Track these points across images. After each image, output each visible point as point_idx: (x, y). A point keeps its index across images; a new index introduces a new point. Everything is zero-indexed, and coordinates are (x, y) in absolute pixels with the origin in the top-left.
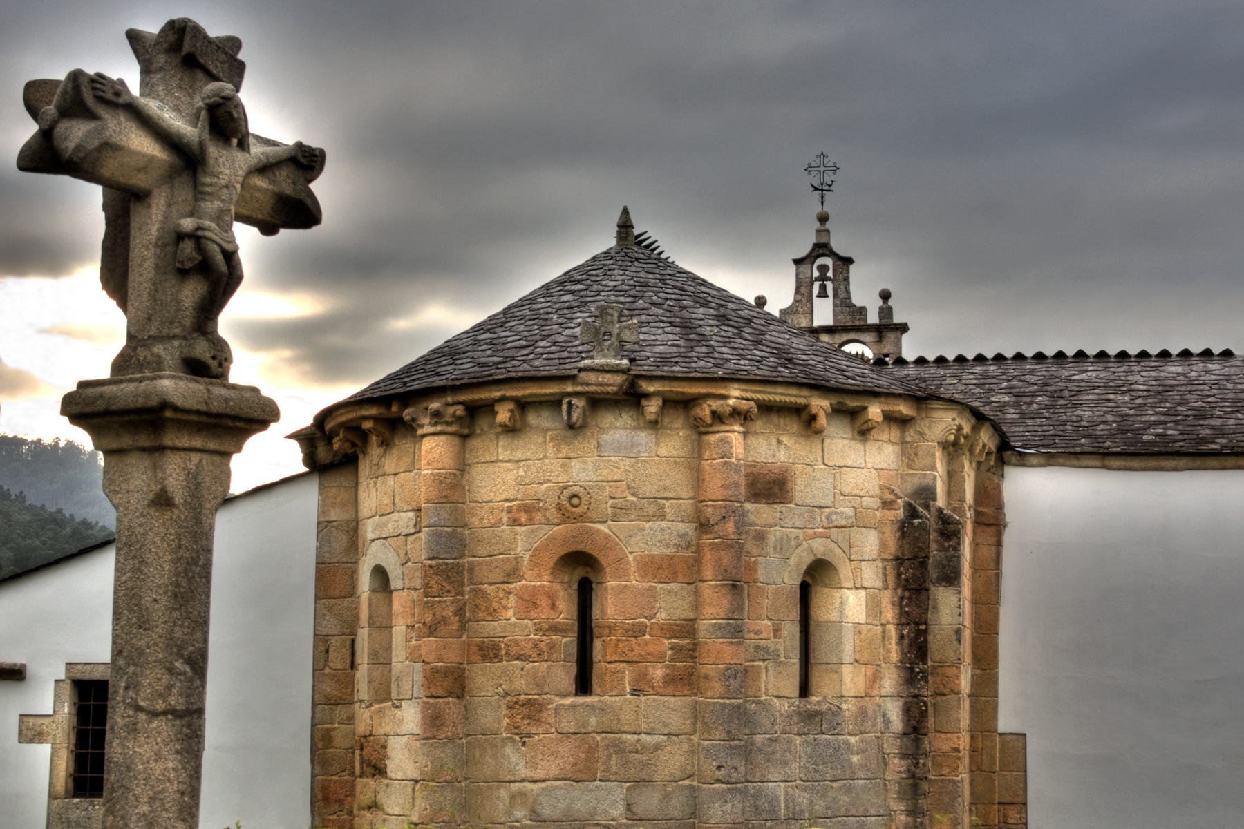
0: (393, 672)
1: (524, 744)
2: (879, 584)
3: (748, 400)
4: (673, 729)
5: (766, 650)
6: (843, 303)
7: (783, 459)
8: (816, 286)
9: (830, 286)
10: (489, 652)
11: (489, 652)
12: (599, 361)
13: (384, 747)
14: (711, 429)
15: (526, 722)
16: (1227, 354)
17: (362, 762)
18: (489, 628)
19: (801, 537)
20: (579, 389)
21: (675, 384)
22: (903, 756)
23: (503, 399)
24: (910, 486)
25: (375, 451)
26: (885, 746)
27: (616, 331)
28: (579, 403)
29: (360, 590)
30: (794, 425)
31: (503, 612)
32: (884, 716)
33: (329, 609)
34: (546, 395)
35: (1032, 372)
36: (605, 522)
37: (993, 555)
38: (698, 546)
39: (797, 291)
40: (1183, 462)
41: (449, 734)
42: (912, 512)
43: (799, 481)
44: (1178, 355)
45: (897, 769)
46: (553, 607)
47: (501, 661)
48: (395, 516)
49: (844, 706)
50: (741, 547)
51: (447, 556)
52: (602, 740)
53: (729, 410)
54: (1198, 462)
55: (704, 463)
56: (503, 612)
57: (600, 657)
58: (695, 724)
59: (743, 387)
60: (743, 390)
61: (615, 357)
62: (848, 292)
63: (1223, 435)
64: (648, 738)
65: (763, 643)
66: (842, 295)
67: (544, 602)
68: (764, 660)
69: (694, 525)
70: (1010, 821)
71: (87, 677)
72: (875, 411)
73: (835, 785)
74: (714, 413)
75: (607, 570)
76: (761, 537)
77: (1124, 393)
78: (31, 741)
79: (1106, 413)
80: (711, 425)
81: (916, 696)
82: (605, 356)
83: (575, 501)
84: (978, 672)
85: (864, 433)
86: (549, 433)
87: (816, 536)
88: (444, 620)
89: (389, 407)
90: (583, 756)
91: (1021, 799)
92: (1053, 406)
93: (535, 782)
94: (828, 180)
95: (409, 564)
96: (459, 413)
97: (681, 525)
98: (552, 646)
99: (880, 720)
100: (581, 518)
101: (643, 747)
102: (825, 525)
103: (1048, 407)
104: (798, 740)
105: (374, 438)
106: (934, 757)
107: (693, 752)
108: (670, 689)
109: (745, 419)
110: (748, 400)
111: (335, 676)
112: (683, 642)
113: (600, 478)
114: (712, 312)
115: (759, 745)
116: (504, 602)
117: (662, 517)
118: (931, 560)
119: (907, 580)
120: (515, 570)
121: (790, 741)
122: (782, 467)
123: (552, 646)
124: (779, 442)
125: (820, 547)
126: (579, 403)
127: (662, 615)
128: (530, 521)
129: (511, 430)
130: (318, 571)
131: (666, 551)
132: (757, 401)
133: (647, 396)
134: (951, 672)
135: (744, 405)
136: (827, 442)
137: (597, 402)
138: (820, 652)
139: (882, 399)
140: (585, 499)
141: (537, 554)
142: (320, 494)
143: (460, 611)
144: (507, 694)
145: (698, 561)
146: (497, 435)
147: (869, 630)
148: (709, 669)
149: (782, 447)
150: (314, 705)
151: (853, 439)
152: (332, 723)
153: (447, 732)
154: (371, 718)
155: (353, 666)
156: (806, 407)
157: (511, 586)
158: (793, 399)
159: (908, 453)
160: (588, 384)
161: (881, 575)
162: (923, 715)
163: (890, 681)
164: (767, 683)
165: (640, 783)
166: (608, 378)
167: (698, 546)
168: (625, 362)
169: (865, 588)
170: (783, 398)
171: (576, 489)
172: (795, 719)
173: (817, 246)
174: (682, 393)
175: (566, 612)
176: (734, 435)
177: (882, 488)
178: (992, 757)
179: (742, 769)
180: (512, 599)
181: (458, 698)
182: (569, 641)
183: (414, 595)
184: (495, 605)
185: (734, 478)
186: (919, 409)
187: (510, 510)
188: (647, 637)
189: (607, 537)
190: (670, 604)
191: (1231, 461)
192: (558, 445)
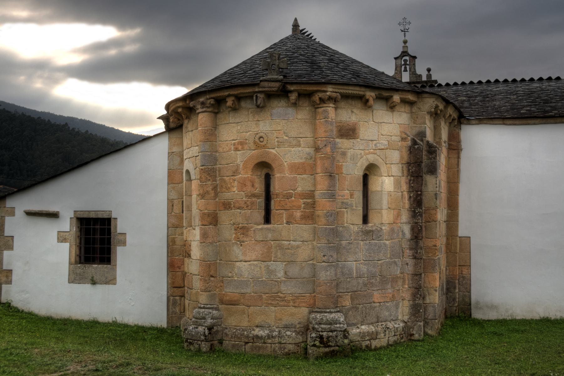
2: (400, 174)
3: (336, 92)
4: (305, 239)
5: (347, 204)
6: (413, 73)
7: (354, 119)
8: (403, 67)
9: (408, 67)
10: (227, 206)
11: (227, 206)
12: (269, 77)
13: (190, 246)
14: (319, 106)
15: (242, 236)
16: (558, 78)
18: (227, 196)
19: (363, 154)
20: (261, 89)
21: (303, 86)
22: (411, 249)
23: (229, 96)
24: (415, 132)
25: (186, 122)
26: (403, 245)
27: (277, 64)
28: (261, 96)
30: (359, 104)
32: (402, 231)
33: (173, 188)
34: (247, 93)
35: (476, 88)
37: (456, 162)
38: (315, 158)
39: (396, 69)
40: (537, 121)
41: (211, 241)
42: (414, 142)
43: (361, 129)
44: (538, 80)
46: (253, 186)
47: (232, 209)
48: (192, 149)
49: (383, 228)
50: (334, 158)
53: (327, 97)
54: (544, 121)
55: (317, 121)
58: (314, 237)
59: (334, 87)
60: (333, 88)
61: (277, 75)
62: (415, 69)
63: (556, 109)
64: (294, 243)
65: (345, 201)
66: (413, 70)
67: (249, 184)
69: (313, 149)
70: (464, 273)
71: (82, 217)
72: (396, 98)
73: (379, 262)
74: (320, 99)
75: (275, 169)
76: (344, 154)
77: (514, 95)
78: (62, 242)
79: (506, 102)
80: (319, 104)
81: (416, 223)
82: (272, 75)
83: (261, 139)
84: (450, 211)
85: (392, 108)
86: (250, 110)
87: (370, 153)
88: (208, 192)
90: (266, 251)
91: (468, 264)
92: (484, 101)
93: (246, 261)
94: (407, 27)
96: (212, 102)
97: (307, 149)
98: (252, 203)
99: (400, 233)
100: (264, 147)
102: (374, 148)
103: (481, 101)
104: (362, 243)
106: (425, 249)
107: (314, 249)
108: (303, 221)
109: (335, 101)
110: (336, 92)
112: (309, 201)
113: (272, 129)
114: (327, 58)
115: (344, 245)
116: (232, 184)
117: (299, 146)
118: (424, 164)
119: (412, 172)
120: (237, 170)
121: (358, 244)
122: (353, 123)
123: (252, 203)
124: (352, 112)
125: (371, 158)
126: (261, 96)
127: (300, 189)
128: (243, 149)
129: (235, 109)
130: (169, 172)
131: (301, 161)
132: (340, 93)
133: (291, 92)
134: (433, 212)
135: (334, 95)
136: (375, 112)
137: (270, 96)
138: (373, 204)
139: (400, 93)
140: (266, 138)
141: (245, 163)
142: (169, 141)
143: (215, 188)
144: (234, 224)
145: (315, 165)
146: (229, 112)
147: (395, 194)
149: (354, 114)
150: (168, 228)
151: (387, 110)
155: (183, 212)
156: (364, 96)
157: (235, 177)
158: (357, 92)
159: (414, 117)
160: (264, 87)
161: (401, 170)
162: (420, 231)
163: (405, 216)
165: (291, 262)
166: (273, 84)
167: (315, 158)
168: (282, 77)
170: (353, 92)
171: (261, 134)
172: (360, 234)
173: (403, 52)
174: (306, 90)
175: (259, 188)
176: (330, 108)
177: (401, 132)
178: (456, 247)
179: (335, 256)
180: (236, 182)
182: (261, 201)
184: (229, 185)
185: (330, 127)
186: (418, 98)
187: (234, 144)
188: (293, 198)
189: (275, 155)
190: (303, 184)
191: (559, 120)
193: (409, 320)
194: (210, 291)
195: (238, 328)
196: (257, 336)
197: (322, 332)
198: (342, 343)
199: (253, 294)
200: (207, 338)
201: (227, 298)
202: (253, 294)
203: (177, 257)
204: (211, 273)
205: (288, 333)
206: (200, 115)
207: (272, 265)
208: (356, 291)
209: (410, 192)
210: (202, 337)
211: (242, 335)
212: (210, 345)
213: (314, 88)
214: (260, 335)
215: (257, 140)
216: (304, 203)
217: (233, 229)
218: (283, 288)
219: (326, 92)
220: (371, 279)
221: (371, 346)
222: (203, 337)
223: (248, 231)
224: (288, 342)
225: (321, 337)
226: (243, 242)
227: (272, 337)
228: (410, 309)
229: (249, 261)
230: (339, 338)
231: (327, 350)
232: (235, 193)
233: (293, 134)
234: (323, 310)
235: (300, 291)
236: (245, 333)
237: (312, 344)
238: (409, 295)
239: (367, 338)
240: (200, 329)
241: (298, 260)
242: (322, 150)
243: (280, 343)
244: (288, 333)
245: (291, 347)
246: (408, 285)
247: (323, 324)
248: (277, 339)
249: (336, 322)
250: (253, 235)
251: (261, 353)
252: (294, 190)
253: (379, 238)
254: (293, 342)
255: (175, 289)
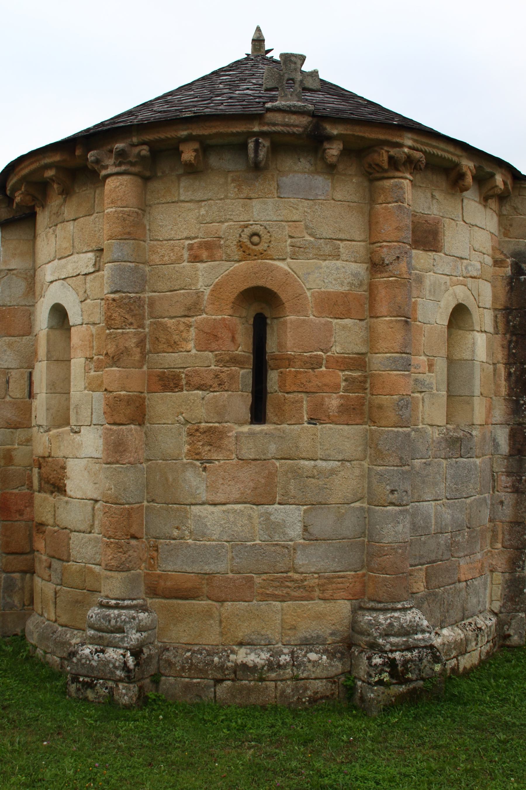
0: (72, 401)
1: (205, 469)
7: (435, 212)
11: (170, 382)
13: (64, 468)
17: (41, 478)
18: (171, 360)
19: (448, 284)
20: (265, 128)
21: (357, 128)
22: (509, 474)
23: (189, 139)
25: (55, 202)
28: (265, 143)
29: (37, 329)
31: (184, 344)
34: (233, 134)
36: (284, 259)
41: (132, 459)
43: (447, 233)
45: (504, 485)
46: (233, 339)
47: (182, 390)
48: (75, 257)
49: (474, 433)
51: (130, 290)
52: (281, 466)
56: (184, 344)
57: (276, 388)
59: (415, 137)
60: (415, 141)
67: (226, 335)
68: (421, 392)
69: (365, 266)
73: (468, 501)
74: (391, 158)
75: (287, 305)
80: (386, 171)
81: (520, 424)
83: (256, 239)
89: (72, 152)
90: (263, 481)
93: (215, 504)
95: (88, 301)
96: (143, 153)
97: (354, 265)
100: (262, 255)
101: (320, 472)
102: (465, 275)
104: (444, 462)
105: (55, 186)
111: (14, 404)
116: (184, 335)
117: (337, 256)
119: (514, 326)
121: (439, 465)
124: (433, 197)
127: (337, 349)
129: (193, 171)
131: (341, 289)
132: (424, 152)
133: (330, 138)
140: (265, 237)
143: (141, 344)
146: (179, 177)
148: (384, 400)
149: (435, 201)
152: (12, 444)
153: (130, 457)
154: (50, 441)
155: (31, 395)
157: (192, 320)
158: (450, 156)
160: (274, 125)
164: (423, 412)
165: (316, 505)
166: (293, 119)
169: (485, 332)
172: (443, 445)
174: (362, 138)
175: (243, 347)
176: (405, 182)
177: (494, 248)
180: (193, 332)
181: (140, 425)
182: (245, 373)
183: (93, 329)
184: (176, 337)
187: (191, 248)
188: (324, 369)
189: (287, 274)
190: (346, 336)
192: (240, 186)
193: (502, 610)
194: (129, 570)
195: (196, 648)
196: (244, 666)
197: (392, 651)
198: (430, 672)
199: (230, 575)
200: (132, 675)
201: (169, 584)
202: (230, 575)
203: (16, 491)
204: (132, 531)
205: (313, 656)
206: (109, 181)
207: (278, 512)
208: (434, 562)
209: (510, 364)
210: (118, 673)
211: (207, 664)
212: (137, 689)
213: (381, 136)
214: (251, 664)
215: (245, 240)
216: (346, 380)
217: (184, 434)
218: (300, 560)
219: (400, 145)
220: (456, 536)
221: (458, 668)
222: (119, 673)
223: (221, 438)
224: (313, 676)
225: (392, 663)
226: (210, 461)
227: (279, 666)
228: (503, 588)
229: (224, 504)
230: (425, 662)
231: (403, 688)
232: (189, 354)
233: (327, 232)
234: (390, 606)
235: (335, 566)
236: (216, 659)
237: (376, 679)
238: (503, 561)
239: (454, 653)
240: (112, 654)
241: (332, 500)
242: (391, 267)
243: (296, 678)
244: (313, 656)
245: (319, 686)
246: (503, 543)
247: (393, 635)
248: (289, 670)
249: (416, 629)
250: (233, 448)
251: (252, 700)
252: (325, 351)
253: (469, 454)
254: (325, 674)
255: (11, 557)
